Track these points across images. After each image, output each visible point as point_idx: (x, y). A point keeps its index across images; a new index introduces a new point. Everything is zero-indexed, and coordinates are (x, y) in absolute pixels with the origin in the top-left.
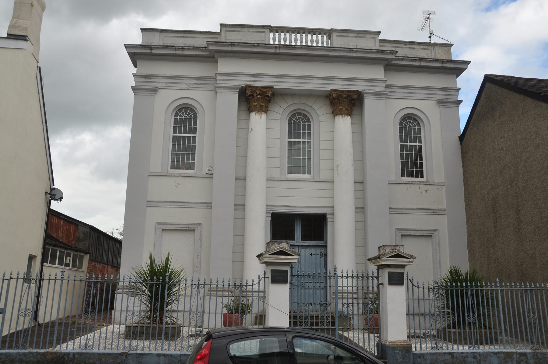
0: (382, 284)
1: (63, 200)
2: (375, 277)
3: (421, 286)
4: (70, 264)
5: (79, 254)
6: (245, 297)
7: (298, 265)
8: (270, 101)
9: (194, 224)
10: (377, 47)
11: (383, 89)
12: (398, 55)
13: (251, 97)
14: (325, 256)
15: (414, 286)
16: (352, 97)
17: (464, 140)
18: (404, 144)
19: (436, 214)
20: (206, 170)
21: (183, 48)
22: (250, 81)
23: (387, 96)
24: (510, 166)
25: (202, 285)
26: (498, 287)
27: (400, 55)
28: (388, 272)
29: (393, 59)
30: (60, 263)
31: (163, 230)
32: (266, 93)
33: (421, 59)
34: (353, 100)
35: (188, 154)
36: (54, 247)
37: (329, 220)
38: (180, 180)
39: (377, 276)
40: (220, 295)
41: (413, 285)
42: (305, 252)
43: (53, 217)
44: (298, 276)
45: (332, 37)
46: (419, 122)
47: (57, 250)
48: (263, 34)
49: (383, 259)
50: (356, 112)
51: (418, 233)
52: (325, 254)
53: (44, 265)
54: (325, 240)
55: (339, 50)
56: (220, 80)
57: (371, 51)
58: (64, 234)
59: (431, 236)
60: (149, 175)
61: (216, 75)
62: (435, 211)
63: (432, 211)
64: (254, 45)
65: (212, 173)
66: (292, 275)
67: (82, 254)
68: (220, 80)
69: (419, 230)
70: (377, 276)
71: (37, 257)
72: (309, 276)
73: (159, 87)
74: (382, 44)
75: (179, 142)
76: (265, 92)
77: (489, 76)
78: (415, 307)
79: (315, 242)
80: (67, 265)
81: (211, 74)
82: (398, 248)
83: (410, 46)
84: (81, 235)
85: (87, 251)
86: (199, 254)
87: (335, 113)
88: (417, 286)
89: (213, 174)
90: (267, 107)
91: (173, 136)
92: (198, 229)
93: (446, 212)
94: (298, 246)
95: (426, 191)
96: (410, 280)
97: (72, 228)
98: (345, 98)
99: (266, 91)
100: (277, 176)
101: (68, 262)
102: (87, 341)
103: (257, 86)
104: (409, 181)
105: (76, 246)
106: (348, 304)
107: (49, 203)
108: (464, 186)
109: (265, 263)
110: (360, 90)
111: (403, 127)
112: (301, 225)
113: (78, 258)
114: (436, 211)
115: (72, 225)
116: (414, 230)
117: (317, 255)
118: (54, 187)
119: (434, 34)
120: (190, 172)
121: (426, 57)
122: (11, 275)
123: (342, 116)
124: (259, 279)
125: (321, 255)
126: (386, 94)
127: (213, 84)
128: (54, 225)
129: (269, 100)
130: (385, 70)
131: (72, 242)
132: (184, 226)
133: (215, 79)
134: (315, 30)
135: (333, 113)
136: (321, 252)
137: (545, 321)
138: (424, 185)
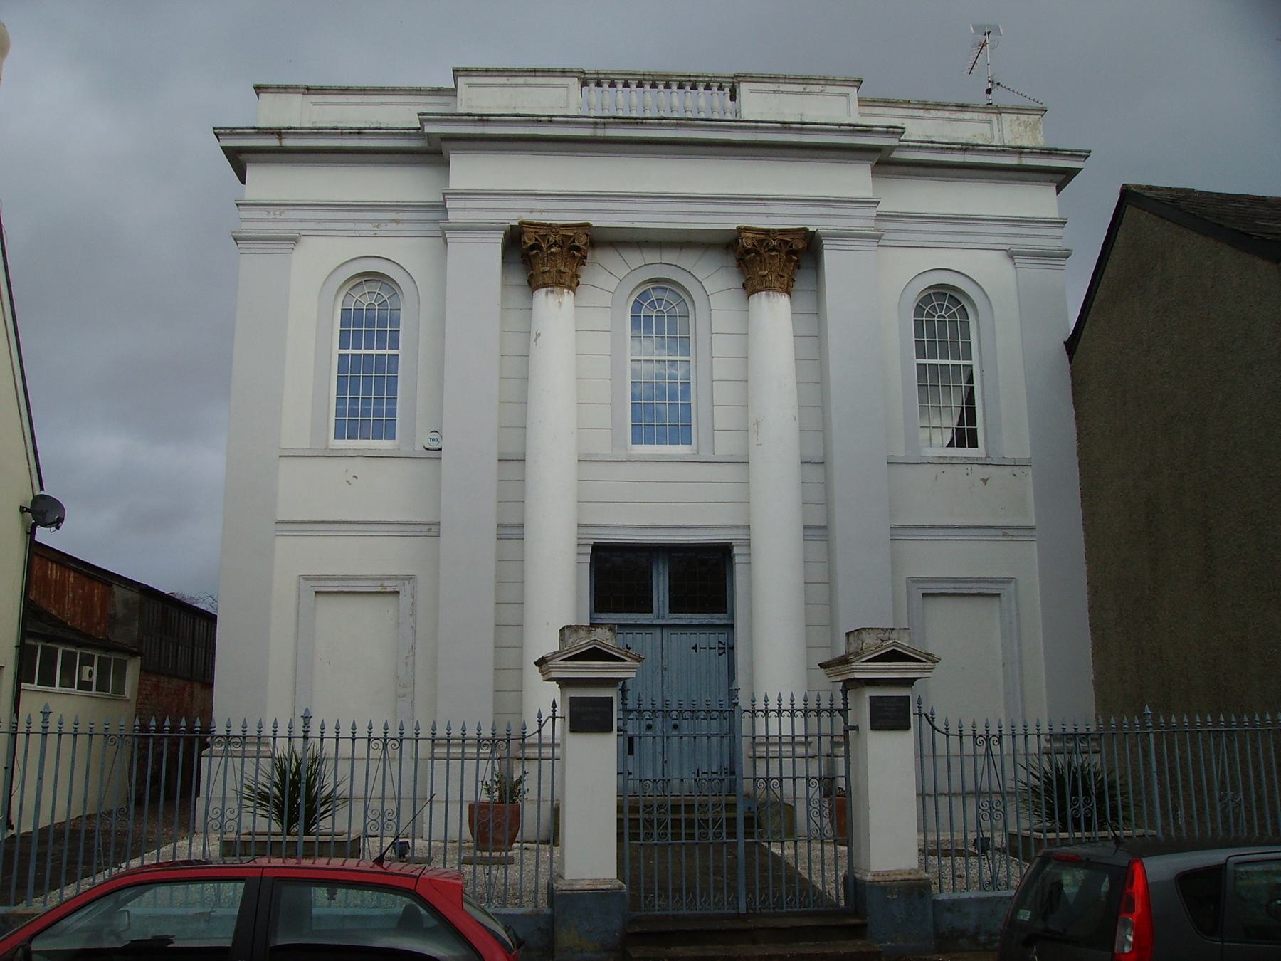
0: (856, 728)
1: (63, 526)
2: (836, 710)
3: (954, 730)
4: (91, 683)
5: (113, 656)
6: (520, 759)
7: (662, 674)
8: (585, 260)
9: (396, 578)
10: (855, 118)
11: (872, 223)
12: (907, 138)
13: (535, 252)
14: (731, 650)
15: (936, 732)
16: (791, 246)
17: (1079, 349)
18: (927, 361)
19: (1010, 538)
20: (423, 439)
21: (359, 132)
22: (532, 211)
23: (881, 243)
24: (1186, 417)
25: (396, 739)
26: (1148, 727)
27: (913, 139)
28: (870, 697)
29: (893, 148)
30: (68, 680)
31: (316, 592)
32: (574, 241)
33: (966, 148)
34: (795, 252)
35: (379, 401)
36: (47, 642)
37: (737, 559)
38: (358, 466)
39: (842, 707)
40: (455, 756)
41: (934, 728)
42: (679, 643)
43: (50, 565)
44: (640, 712)
45: (740, 93)
46: (966, 306)
47: (57, 650)
48: (563, 91)
49: (855, 665)
50: (803, 281)
51: (965, 589)
52: (731, 646)
53: (22, 688)
54: (728, 611)
55: (756, 128)
56: (455, 210)
57: (839, 128)
58: (77, 608)
59: (999, 595)
60: (280, 456)
61: (444, 199)
62: (1006, 532)
63: (1000, 532)
64: (539, 119)
65: (439, 447)
66: (625, 711)
67: (121, 657)
68: (455, 210)
69: (967, 582)
70: (842, 707)
71: (5, 669)
72: (722, 711)
73: (302, 233)
74: (867, 110)
75: (356, 369)
76: (571, 236)
77: (1133, 189)
78: (966, 773)
79: (705, 615)
80: (85, 686)
81: (436, 198)
82: (894, 635)
83: (940, 114)
84: (120, 610)
85: (135, 650)
86: (409, 652)
87: (750, 288)
88: (944, 731)
89: (440, 449)
90: (577, 276)
91: (340, 355)
92: (406, 591)
93: (1035, 533)
94: (662, 626)
95: (985, 481)
96: (926, 715)
97: (96, 591)
98: (774, 249)
99: (572, 234)
100: (605, 451)
101: (85, 677)
102: (385, 757)
103: (549, 222)
104: (940, 457)
105: (107, 637)
106: (768, 779)
107: (31, 533)
108: (1080, 466)
109: (557, 680)
110: (811, 229)
111: (924, 319)
112: (669, 574)
113: (112, 665)
114: (1009, 532)
115: (96, 584)
116: (955, 580)
117: (711, 648)
118: (42, 493)
119: (998, 84)
120: (383, 445)
121: (980, 142)
122: (1026, 728)
123: (768, 296)
124: (540, 722)
125: (720, 648)
126: (879, 238)
127: (436, 221)
128: (53, 583)
129: (581, 258)
130: (874, 173)
131: (99, 628)
132: (370, 583)
133: (442, 208)
134: (694, 79)
135: (744, 286)
136: (720, 642)
137: (1274, 815)
138: (980, 467)
